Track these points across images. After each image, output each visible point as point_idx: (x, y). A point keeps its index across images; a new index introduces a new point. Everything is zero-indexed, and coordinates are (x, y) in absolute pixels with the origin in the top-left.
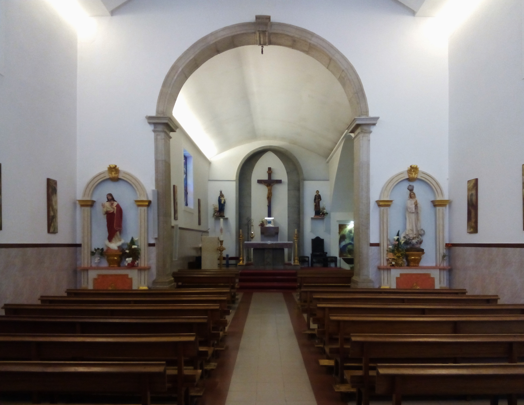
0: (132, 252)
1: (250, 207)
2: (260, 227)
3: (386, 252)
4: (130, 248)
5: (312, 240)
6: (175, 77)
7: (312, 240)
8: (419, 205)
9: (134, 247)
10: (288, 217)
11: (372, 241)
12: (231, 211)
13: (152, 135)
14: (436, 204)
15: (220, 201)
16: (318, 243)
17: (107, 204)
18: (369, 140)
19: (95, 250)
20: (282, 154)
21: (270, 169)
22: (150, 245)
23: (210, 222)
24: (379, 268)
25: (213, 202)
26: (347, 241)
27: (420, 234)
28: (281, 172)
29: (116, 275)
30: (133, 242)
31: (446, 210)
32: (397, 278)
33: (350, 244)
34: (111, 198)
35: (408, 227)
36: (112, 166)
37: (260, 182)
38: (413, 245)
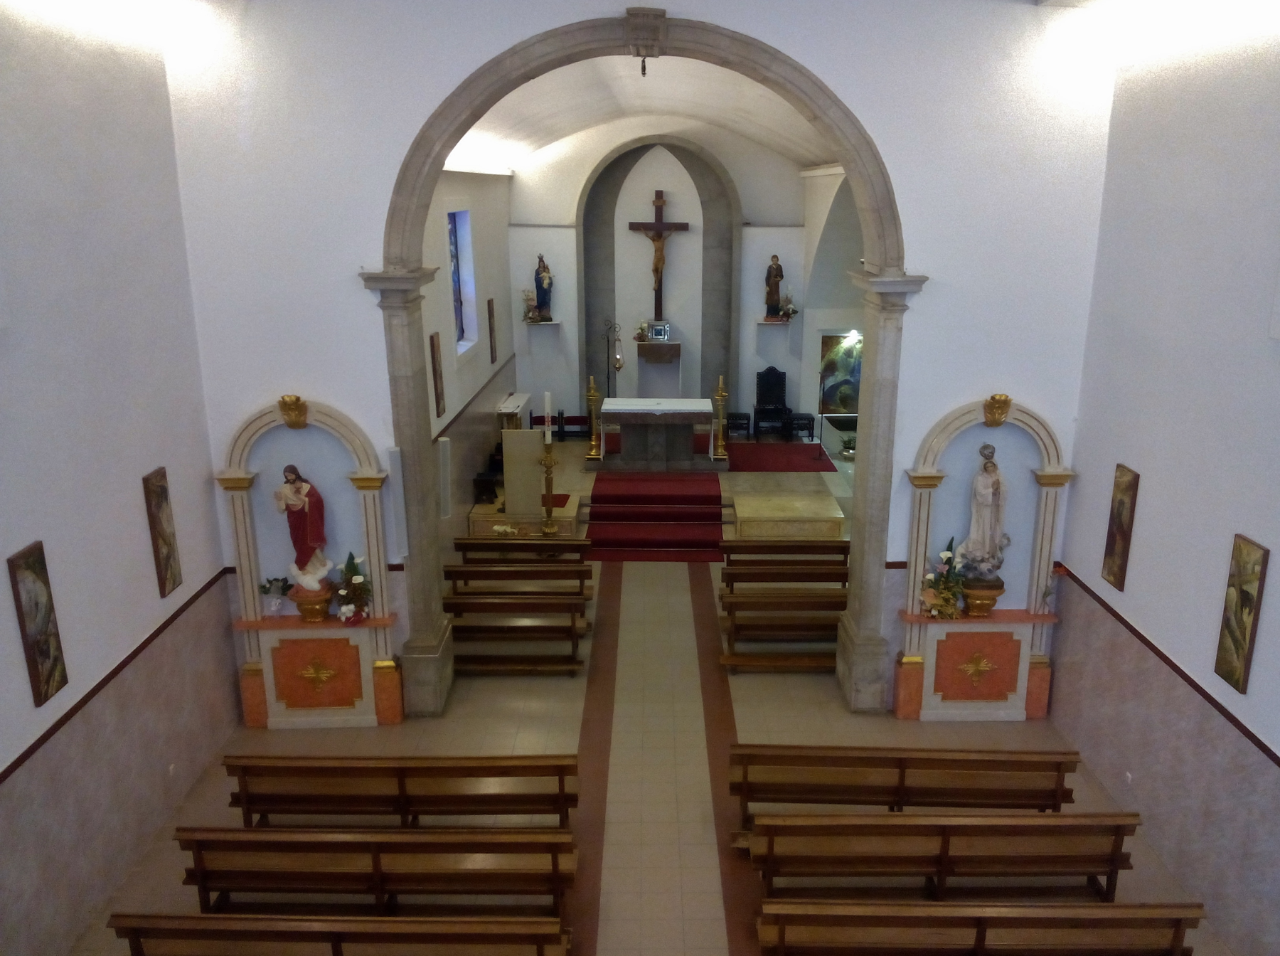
0: (351, 591)
1: (613, 291)
2: (636, 343)
3: (919, 585)
4: (348, 584)
5: (759, 374)
6: (427, 168)
7: (759, 374)
8: (1002, 488)
9: (358, 579)
10: (704, 315)
11: (891, 558)
12: (566, 307)
13: (379, 315)
14: (1042, 481)
15: (539, 281)
16: (772, 383)
17: (287, 490)
18: (900, 329)
19: (270, 582)
20: (690, 154)
21: (659, 195)
22: (393, 568)
23: (516, 331)
24: (902, 613)
25: (524, 283)
26: (840, 376)
27: (997, 552)
28: (687, 204)
29: (321, 640)
30: (352, 568)
31: (1064, 491)
32: (939, 642)
33: (846, 382)
34: (293, 475)
35: (974, 534)
36: (287, 399)
37: (634, 227)
38: (981, 574)
